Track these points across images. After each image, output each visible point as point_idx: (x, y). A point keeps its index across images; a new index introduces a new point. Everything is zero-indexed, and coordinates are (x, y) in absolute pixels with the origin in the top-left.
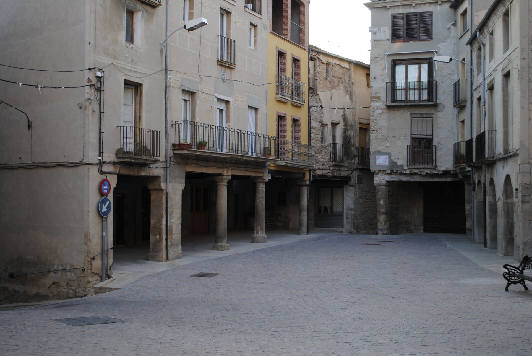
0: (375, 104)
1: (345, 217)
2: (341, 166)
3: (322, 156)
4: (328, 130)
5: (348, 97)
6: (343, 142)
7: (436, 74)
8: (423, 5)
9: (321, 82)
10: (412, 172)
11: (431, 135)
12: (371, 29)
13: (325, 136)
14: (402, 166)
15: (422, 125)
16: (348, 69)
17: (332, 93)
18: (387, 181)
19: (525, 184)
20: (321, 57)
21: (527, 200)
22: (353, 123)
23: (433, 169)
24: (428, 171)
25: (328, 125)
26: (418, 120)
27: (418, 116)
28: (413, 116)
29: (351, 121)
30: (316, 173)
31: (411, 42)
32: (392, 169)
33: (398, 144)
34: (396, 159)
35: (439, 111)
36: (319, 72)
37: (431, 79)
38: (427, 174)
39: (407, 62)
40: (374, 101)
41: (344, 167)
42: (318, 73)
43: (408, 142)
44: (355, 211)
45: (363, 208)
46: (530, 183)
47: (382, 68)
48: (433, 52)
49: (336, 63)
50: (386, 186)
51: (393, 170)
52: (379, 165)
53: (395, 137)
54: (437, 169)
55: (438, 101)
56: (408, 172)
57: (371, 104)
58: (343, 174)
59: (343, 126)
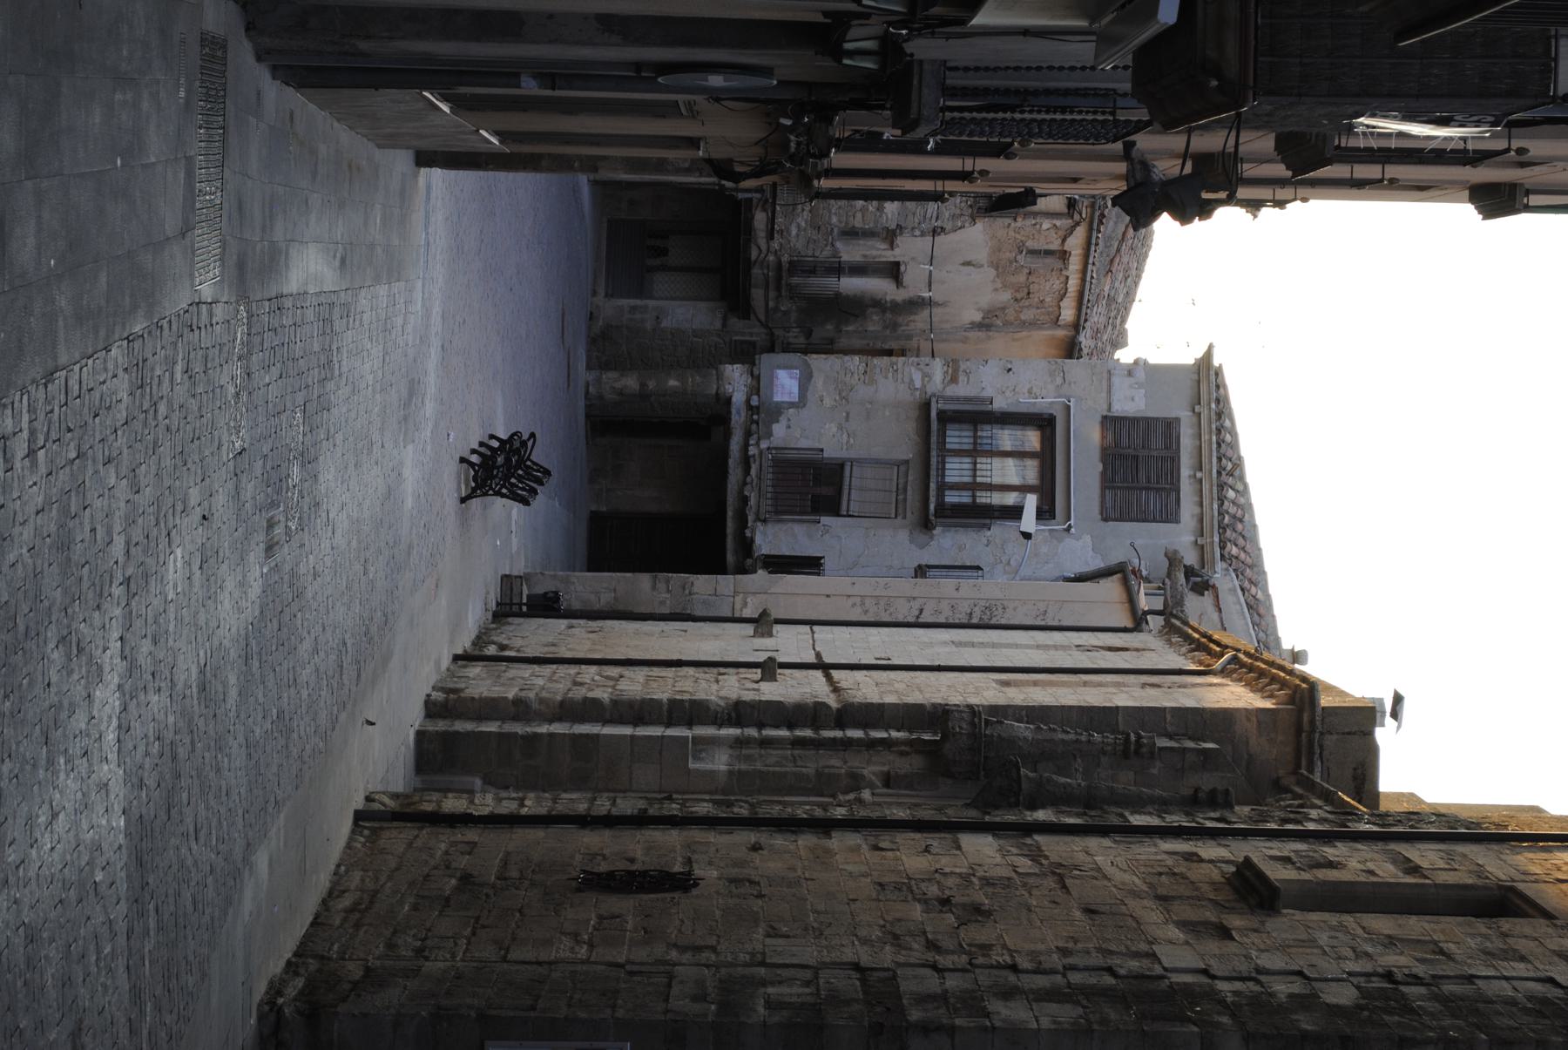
0: (938, 369)
1: (638, 302)
2: (778, 289)
3: (805, 230)
4: (878, 249)
5: (978, 317)
6: (847, 297)
7: (1011, 526)
8: (1197, 499)
9: (1012, 233)
10: (752, 460)
11: (848, 511)
12: (1142, 363)
13: (861, 242)
14: (769, 435)
15: (877, 490)
16: (1058, 319)
17: (982, 266)
18: (731, 397)
19: (692, 583)
20: (1080, 232)
21: (658, 585)
22: (904, 331)
23: (757, 514)
24: (752, 502)
25: (892, 249)
26: (891, 480)
27: (901, 481)
28: (903, 468)
29: (907, 325)
30: (757, 212)
31: (1100, 467)
32: (761, 410)
33: (827, 426)
34: (789, 420)
35: (911, 533)
36: (1038, 226)
37: (996, 514)
38: (744, 500)
39: (1047, 458)
40: (945, 368)
41: (777, 298)
42: (1035, 225)
43: (832, 452)
44: (654, 330)
45: (663, 360)
46: (694, 594)
47: (1035, 390)
48: (1069, 519)
49: (1070, 282)
50: (717, 394)
51: (758, 414)
52: (772, 378)
53: (847, 420)
54: (759, 524)
55: (938, 531)
56: (752, 451)
57: (938, 359)
58: (757, 294)
59: (892, 297)
